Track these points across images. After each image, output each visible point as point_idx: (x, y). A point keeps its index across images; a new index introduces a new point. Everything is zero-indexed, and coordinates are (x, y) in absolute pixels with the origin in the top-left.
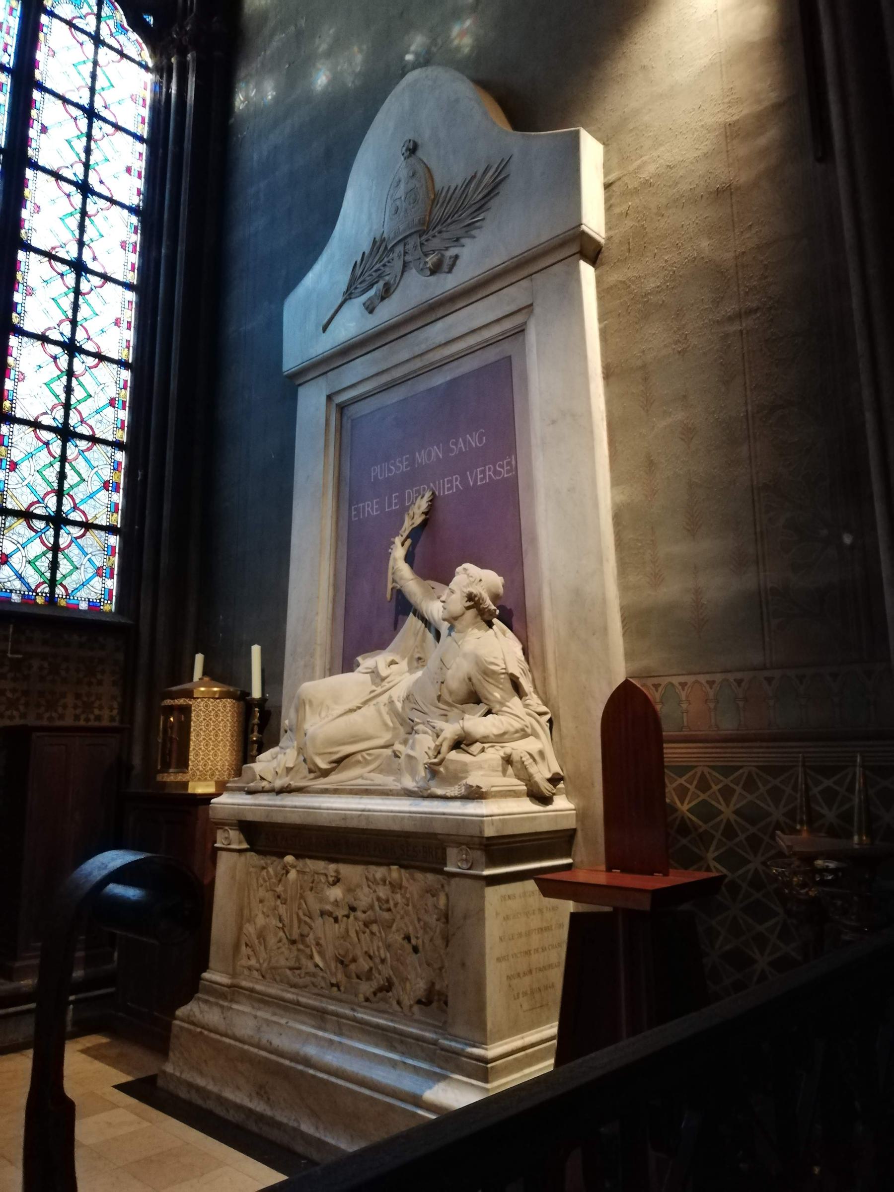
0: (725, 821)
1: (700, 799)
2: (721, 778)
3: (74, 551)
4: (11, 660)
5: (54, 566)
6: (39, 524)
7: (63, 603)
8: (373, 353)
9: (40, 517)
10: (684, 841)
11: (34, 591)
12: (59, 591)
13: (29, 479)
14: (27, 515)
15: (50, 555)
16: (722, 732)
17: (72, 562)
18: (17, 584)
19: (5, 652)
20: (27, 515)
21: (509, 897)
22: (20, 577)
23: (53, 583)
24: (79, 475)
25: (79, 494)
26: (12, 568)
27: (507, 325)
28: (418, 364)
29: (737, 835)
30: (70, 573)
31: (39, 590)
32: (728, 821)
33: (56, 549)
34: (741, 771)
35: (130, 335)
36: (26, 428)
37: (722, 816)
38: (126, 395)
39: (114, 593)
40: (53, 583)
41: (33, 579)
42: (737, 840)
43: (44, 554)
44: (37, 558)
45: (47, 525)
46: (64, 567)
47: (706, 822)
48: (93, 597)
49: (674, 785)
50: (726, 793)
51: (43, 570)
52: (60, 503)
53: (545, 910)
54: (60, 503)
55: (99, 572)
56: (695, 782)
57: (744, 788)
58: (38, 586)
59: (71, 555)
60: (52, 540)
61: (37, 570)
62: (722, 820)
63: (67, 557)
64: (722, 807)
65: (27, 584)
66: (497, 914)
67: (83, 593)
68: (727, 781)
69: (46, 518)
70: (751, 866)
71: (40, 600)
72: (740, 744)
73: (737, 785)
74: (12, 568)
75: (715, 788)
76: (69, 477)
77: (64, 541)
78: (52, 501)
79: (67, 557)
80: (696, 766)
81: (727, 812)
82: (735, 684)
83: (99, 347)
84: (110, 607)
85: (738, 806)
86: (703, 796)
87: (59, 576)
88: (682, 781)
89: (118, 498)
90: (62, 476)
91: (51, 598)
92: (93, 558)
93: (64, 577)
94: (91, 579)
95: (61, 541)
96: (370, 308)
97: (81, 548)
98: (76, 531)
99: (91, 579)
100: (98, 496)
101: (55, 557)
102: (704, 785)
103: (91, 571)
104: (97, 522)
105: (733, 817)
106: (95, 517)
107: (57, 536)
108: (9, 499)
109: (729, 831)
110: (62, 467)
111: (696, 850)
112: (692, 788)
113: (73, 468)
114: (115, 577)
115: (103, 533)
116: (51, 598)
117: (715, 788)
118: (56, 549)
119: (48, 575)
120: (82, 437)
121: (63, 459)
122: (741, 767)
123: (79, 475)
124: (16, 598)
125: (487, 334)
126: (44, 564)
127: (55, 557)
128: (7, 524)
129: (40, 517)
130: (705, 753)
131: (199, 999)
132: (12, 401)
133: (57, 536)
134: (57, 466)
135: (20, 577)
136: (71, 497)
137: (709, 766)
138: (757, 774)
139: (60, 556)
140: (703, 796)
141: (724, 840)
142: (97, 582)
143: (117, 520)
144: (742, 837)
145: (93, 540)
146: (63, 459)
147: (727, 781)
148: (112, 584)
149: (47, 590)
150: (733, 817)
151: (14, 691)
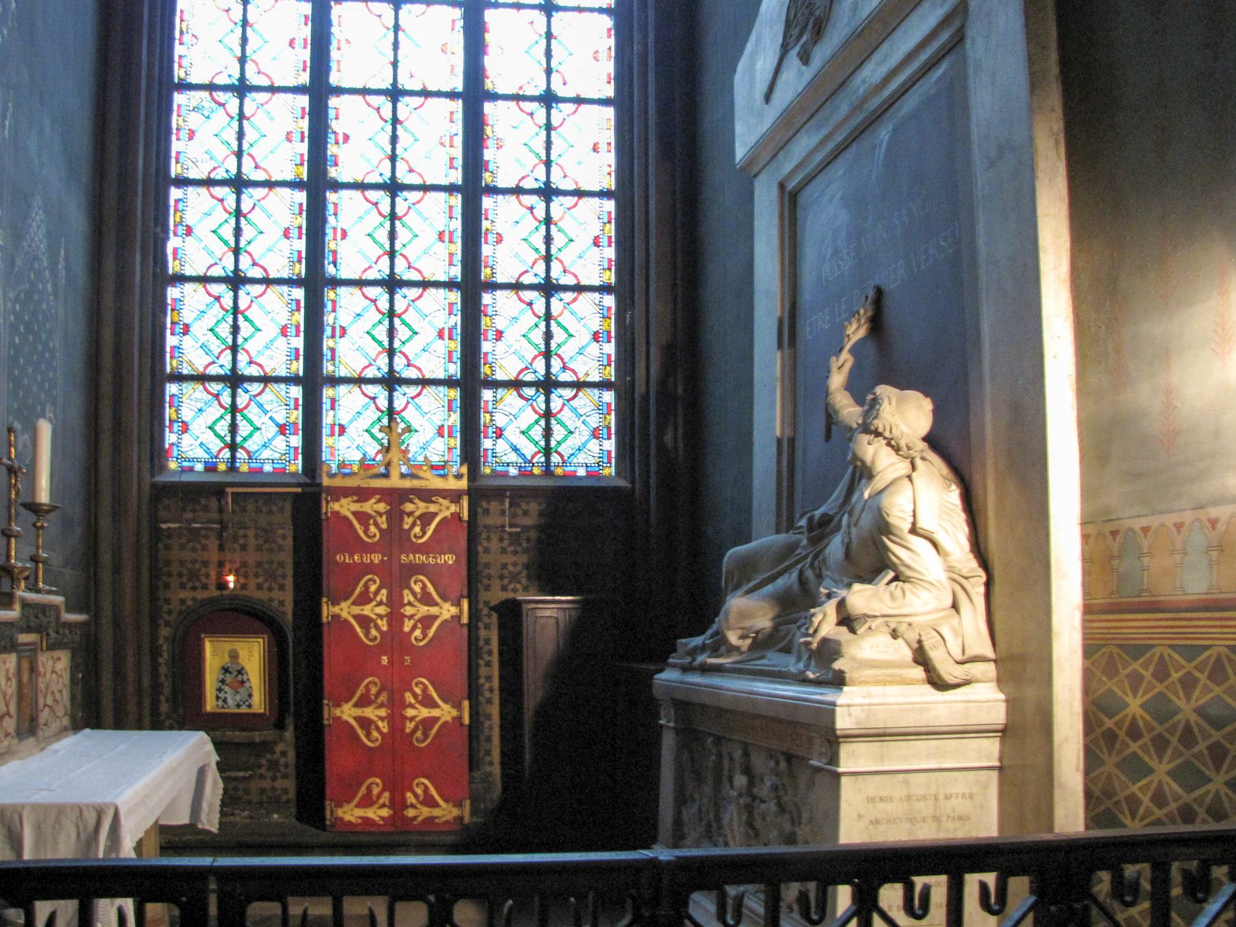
0: (1183, 722)
1: (1156, 691)
2: (1183, 662)
3: (566, 416)
4: (510, 534)
5: (548, 433)
6: (529, 392)
7: (559, 471)
8: (820, 113)
9: (529, 384)
10: (1134, 747)
11: (530, 462)
12: (555, 459)
13: (516, 346)
14: (516, 384)
15: (543, 423)
16: (1190, 597)
17: (565, 427)
18: (513, 457)
19: (503, 526)
20: (516, 384)
21: (882, 799)
22: (515, 449)
23: (547, 451)
24: (566, 330)
25: (567, 351)
26: (507, 441)
27: (945, 36)
28: (859, 117)
29: (1196, 743)
30: (565, 439)
31: (535, 461)
32: (1188, 722)
33: (548, 415)
34: (1207, 654)
35: (609, 67)
36: (506, 293)
37: (1179, 716)
38: (611, 229)
39: (613, 455)
40: (547, 451)
41: (529, 449)
42: (1196, 749)
43: (537, 422)
44: (530, 427)
45: (538, 391)
46: (558, 432)
47: (1161, 723)
48: (591, 461)
49: (1127, 671)
50: (1188, 683)
51: (537, 439)
52: (548, 366)
53: (944, 819)
54: (548, 366)
55: (595, 434)
56: (1152, 668)
57: (1210, 678)
58: (533, 457)
59: (564, 419)
60: (543, 406)
61: (531, 440)
62: (1179, 721)
63: (560, 423)
64: (1181, 703)
65: (522, 456)
66: (860, 816)
67: (581, 458)
68: (1189, 667)
69: (535, 384)
70: (1211, 787)
71: (536, 471)
72: (1208, 615)
73: (1202, 673)
74: (507, 441)
75: (1175, 676)
76: (555, 336)
77: (555, 405)
78: (540, 365)
79: (560, 423)
80: (1154, 646)
81: (1134, 705)
82: (1208, 525)
83: (576, 183)
84: (610, 471)
85: (1201, 702)
86: (1159, 688)
87: (553, 443)
88: (1136, 666)
89: (610, 348)
90: (548, 336)
91: (548, 471)
92: (588, 419)
93: (559, 443)
94: (587, 441)
95: (552, 405)
96: (805, 58)
97: (574, 410)
98: (568, 393)
99: (587, 441)
100: (588, 350)
101: (548, 424)
102: (1162, 673)
103: (586, 434)
104: (589, 379)
105: (1193, 718)
106: (587, 374)
107: (548, 402)
108: (498, 369)
109: (1188, 738)
110: (548, 326)
111: (1146, 759)
112: (1147, 675)
113: (559, 325)
114: (613, 436)
115: (596, 391)
116: (548, 471)
117: (1175, 676)
118: (548, 415)
119: (543, 443)
120: (566, 288)
121: (548, 317)
122: (1207, 648)
123: (566, 330)
124: (513, 471)
125: (923, 57)
126: (537, 432)
127: (548, 424)
128: (499, 397)
129: (529, 384)
130: (1166, 627)
131: (451, 833)
132: (492, 269)
133: (548, 402)
134: (543, 325)
135: (515, 449)
136: (559, 356)
137: (1169, 646)
138: (1228, 658)
139: (553, 421)
140: (1159, 688)
141: (1182, 748)
142: (594, 445)
143: (611, 373)
144: (1202, 746)
145: (586, 400)
146: (548, 317)
147: (1189, 667)
148: (610, 445)
149: (543, 459)
150: (1193, 718)
151: (514, 564)
